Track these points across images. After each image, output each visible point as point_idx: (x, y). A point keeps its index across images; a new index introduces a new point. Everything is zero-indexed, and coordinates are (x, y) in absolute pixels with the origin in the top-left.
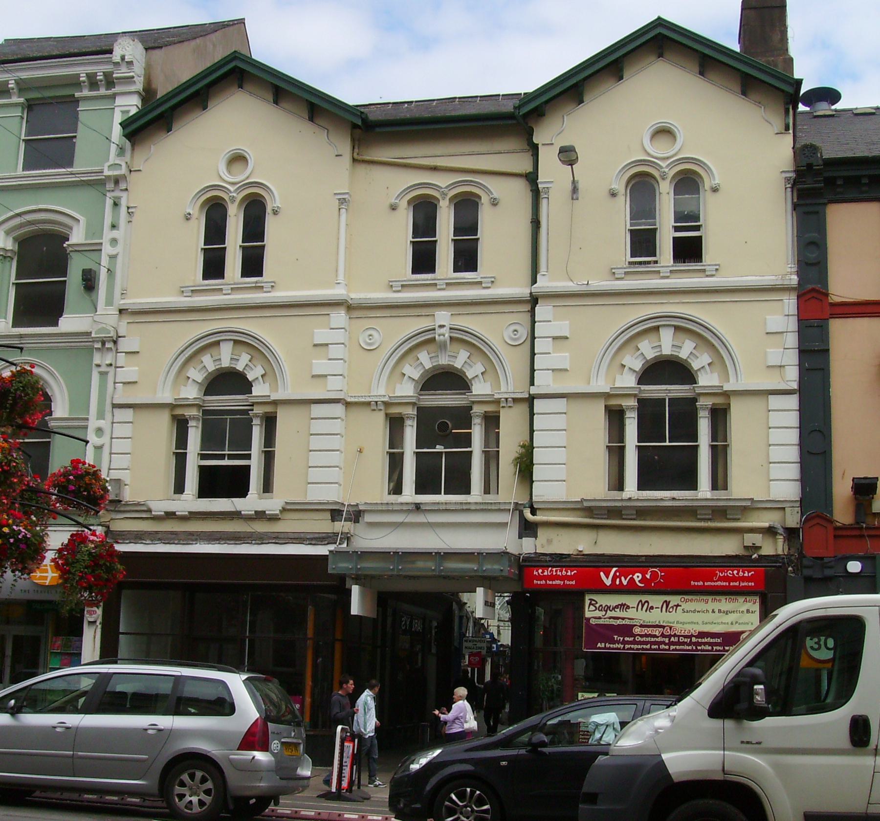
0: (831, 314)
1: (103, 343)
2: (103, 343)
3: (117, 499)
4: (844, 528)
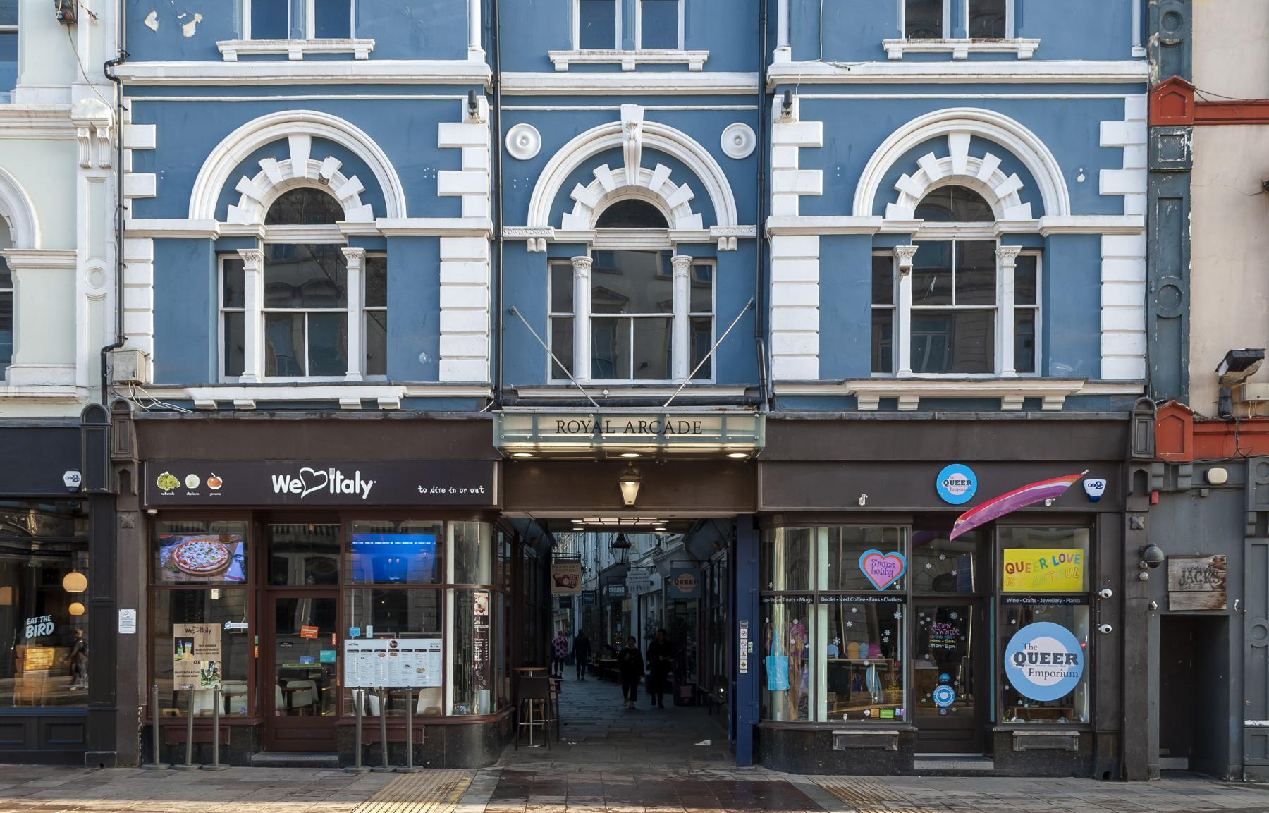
0: (1195, 120)
1: (93, 132)
2: (93, 132)
3: (134, 379)
4: (1205, 422)
